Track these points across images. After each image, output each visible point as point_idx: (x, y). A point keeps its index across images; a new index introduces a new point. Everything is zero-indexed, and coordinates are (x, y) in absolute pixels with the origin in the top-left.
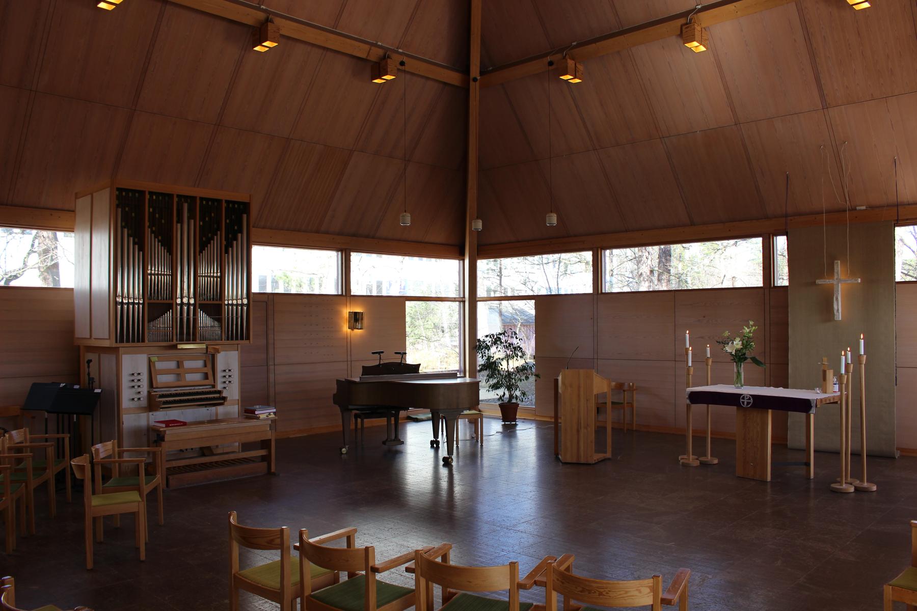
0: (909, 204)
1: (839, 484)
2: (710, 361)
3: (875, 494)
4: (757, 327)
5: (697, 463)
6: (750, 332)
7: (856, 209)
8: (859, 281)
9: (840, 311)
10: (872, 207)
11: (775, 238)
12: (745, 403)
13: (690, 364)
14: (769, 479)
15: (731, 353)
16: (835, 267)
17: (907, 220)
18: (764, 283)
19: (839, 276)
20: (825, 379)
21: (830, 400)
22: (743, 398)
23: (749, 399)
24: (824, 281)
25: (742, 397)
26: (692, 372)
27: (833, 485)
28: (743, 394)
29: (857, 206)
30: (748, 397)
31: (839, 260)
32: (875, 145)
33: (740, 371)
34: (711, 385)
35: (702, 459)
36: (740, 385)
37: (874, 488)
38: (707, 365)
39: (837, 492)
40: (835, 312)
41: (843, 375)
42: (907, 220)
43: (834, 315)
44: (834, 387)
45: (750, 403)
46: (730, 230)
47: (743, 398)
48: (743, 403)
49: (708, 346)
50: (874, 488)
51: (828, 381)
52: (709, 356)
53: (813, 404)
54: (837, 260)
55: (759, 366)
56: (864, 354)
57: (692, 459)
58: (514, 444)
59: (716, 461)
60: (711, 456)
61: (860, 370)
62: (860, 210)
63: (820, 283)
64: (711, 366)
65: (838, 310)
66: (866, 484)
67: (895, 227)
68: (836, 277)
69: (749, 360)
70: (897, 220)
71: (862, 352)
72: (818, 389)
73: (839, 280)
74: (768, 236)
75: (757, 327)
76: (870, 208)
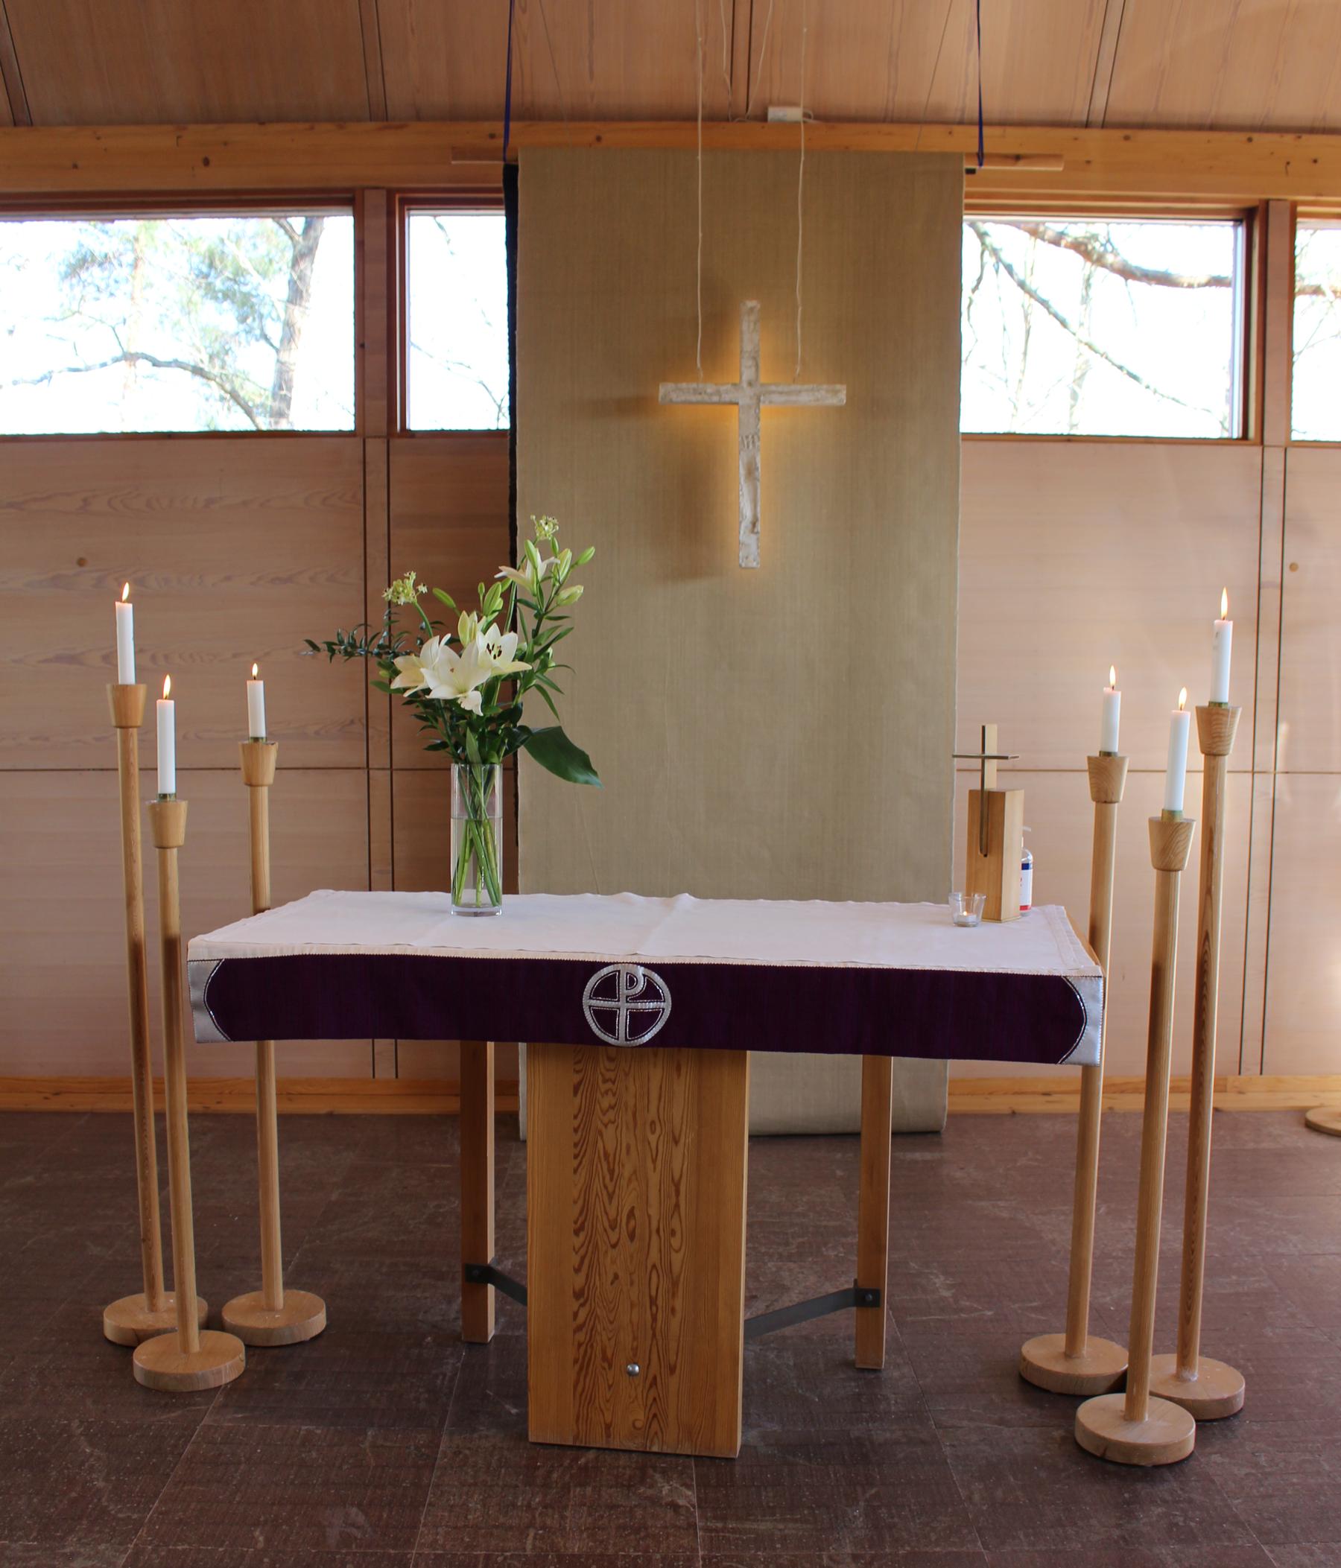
2: (271, 758)
4: (591, 552)
7: (763, 118)
10: (823, 118)
12: (622, 1022)
13: (168, 781)
22: (607, 989)
23: (651, 992)
24: (696, 392)
25: (593, 981)
26: (178, 831)
28: (596, 966)
29: (771, 103)
30: (641, 986)
38: (252, 784)
45: (653, 1016)
46: (206, 162)
48: (607, 1019)
49: (255, 670)
55: (564, 775)
58: (317, 223)
64: (271, 789)
68: (748, 374)
74: (383, 201)
76: (817, 118)
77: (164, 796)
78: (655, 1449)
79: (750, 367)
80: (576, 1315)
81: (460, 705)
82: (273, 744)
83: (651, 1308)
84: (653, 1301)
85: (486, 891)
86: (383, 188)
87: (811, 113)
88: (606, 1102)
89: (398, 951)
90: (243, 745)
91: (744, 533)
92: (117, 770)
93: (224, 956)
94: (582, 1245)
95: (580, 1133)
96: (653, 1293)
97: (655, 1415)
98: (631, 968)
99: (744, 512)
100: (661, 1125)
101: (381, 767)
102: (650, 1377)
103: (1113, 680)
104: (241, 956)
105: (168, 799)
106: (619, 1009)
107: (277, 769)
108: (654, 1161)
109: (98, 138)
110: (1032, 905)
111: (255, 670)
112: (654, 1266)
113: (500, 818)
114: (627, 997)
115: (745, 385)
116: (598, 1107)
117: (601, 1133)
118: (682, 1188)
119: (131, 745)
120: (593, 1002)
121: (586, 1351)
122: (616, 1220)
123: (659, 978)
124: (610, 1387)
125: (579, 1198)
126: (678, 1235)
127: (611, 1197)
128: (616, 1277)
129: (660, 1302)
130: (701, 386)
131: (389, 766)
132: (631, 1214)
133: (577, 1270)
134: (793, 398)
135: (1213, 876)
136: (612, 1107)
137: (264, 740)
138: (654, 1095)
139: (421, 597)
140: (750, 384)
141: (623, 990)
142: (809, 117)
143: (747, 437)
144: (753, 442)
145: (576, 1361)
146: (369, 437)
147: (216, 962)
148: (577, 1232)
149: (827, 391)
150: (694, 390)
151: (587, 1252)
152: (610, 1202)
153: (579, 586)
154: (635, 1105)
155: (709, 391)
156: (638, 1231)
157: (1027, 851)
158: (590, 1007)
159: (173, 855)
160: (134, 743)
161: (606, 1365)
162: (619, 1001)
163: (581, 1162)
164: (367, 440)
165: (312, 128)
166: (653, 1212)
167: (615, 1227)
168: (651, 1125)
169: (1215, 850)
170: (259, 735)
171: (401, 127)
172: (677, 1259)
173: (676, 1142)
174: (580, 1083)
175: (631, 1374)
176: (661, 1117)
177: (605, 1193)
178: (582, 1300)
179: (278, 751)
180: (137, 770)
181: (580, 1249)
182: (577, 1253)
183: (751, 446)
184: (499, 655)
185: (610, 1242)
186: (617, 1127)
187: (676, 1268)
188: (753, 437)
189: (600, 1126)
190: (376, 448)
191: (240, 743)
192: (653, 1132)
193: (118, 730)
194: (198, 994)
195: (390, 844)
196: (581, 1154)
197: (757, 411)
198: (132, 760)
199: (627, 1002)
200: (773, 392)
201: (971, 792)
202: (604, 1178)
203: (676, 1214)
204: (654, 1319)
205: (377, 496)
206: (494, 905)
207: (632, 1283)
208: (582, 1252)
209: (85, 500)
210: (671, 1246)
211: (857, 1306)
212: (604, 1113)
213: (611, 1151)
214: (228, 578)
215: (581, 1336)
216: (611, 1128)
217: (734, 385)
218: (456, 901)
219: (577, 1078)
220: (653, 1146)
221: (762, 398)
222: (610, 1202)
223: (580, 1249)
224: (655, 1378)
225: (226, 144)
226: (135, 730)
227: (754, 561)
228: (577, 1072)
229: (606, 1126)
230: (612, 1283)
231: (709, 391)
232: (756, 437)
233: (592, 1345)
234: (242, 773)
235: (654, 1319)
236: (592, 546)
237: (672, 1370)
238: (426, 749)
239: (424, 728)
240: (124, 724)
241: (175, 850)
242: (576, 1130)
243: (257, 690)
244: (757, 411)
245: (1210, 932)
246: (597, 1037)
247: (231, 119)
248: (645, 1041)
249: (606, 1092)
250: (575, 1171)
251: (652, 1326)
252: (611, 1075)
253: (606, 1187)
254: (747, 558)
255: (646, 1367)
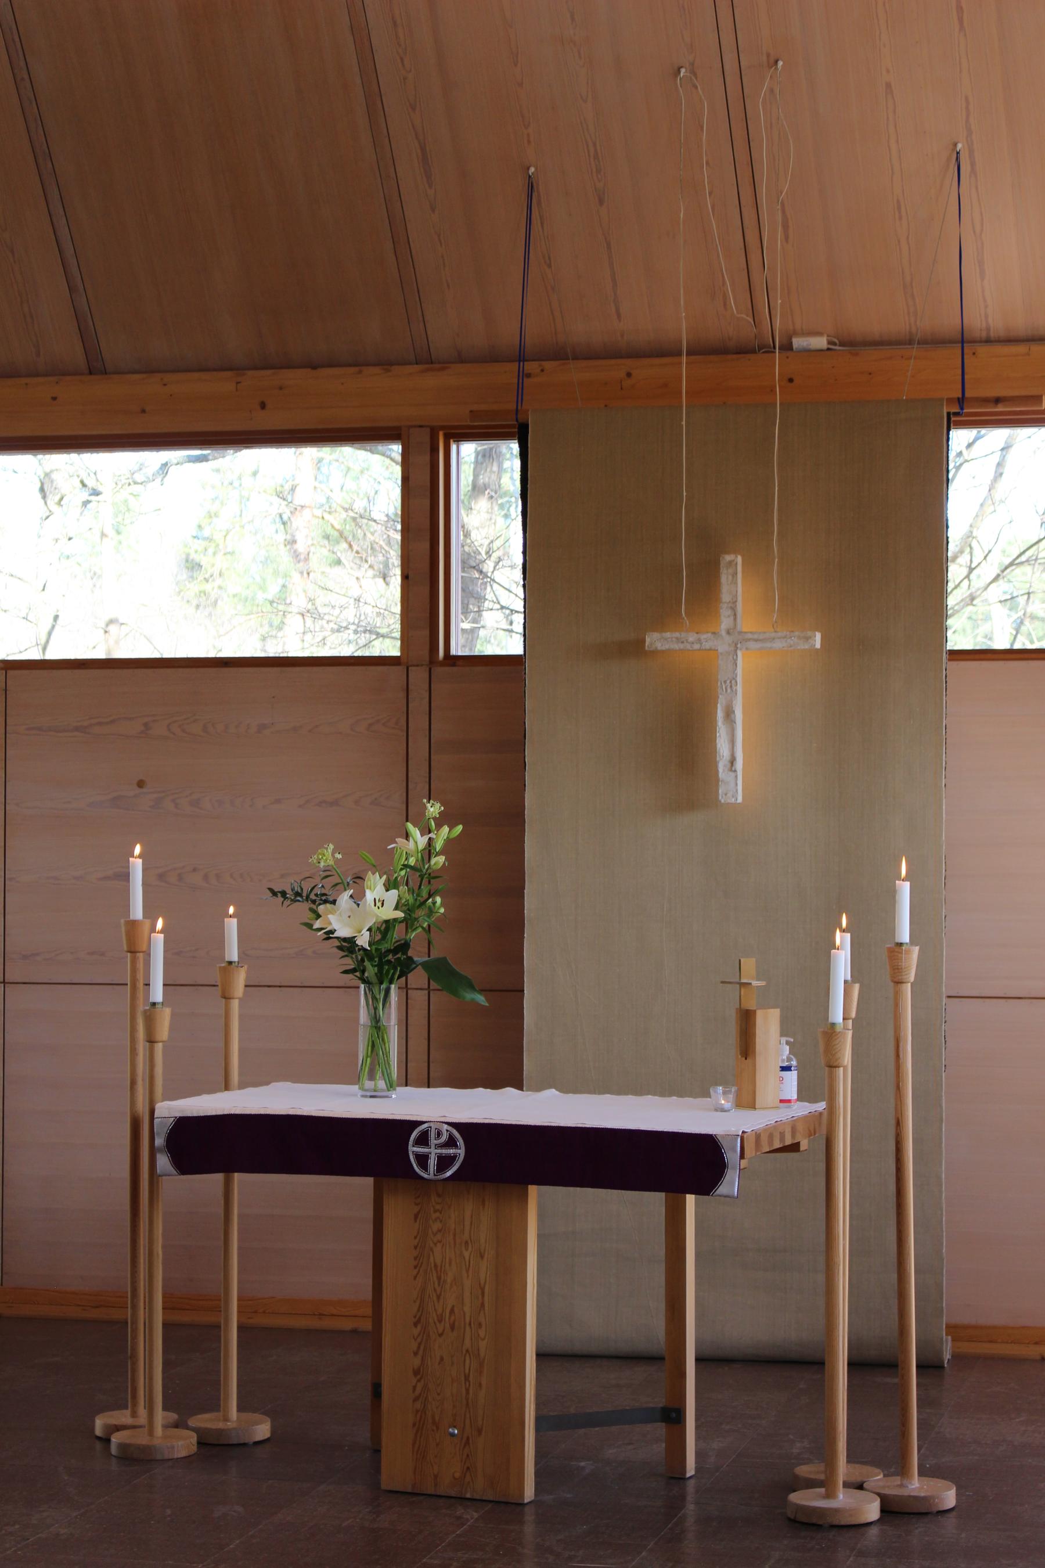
0: (988, 341)
1: (823, 1490)
2: (240, 979)
3: (950, 1523)
4: (460, 828)
5: (184, 1444)
6: (429, 850)
8: (818, 645)
9: (739, 765)
11: (454, 447)
12: (432, 1162)
13: (157, 994)
14: (529, 1493)
15: (348, 945)
16: (724, 579)
17: (997, 401)
18: (406, 639)
19: (739, 621)
20: (747, 1047)
21: (782, 1135)
22: (423, 1139)
23: (451, 1142)
24: (678, 640)
25: (415, 1134)
26: (163, 1031)
27: (797, 1498)
29: (795, 333)
30: (444, 1138)
31: (735, 552)
32: (888, 85)
33: (384, 1022)
34: (242, 1086)
35: (204, 1421)
36: (381, 1084)
37: (949, 1498)
38: (227, 997)
39: (818, 1527)
40: (721, 770)
41: (839, 1028)
42: (997, 401)
43: (717, 780)
44: (782, 1079)
46: (263, 406)
47: (423, 1139)
48: (423, 1160)
49: (231, 910)
50: (949, 1498)
51: (760, 1060)
52: (235, 957)
53: (731, 1156)
54: (728, 553)
56: (913, 940)
57: (165, 1427)
59: (263, 1430)
60: (240, 1409)
61: (896, 1005)
62: (808, 352)
63: (660, 646)
65: (732, 761)
66: (916, 1485)
67: (949, 430)
68: (725, 623)
69: (418, 977)
70: (961, 401)
71: (904, 934)
72: (720, 1089)
73: (739, 640)
75: (460, 828)
77: (154, 1004)
78: (468, 1496)
79: (729, 616)
80: (414, 1388)
81: (355, 941)
82: (242, 967)
83: (465, 1383)
84: (467, 1378)
85: (383, 1081)
86: (426, 426)
87: (836, 341)
88: (436, 1226)
89: (291, 1112)
90: (220, 967)
91: (724, 770)
92: (127, 984)
93: (178, 1115)
94: (419, 1334)
95: (418, 1250)
96: (467, 1371)
97: (468, 1468)
98: (438, 1126)
99: (721, 751)
100: (472, 1244)
101: (419, 987)
102: (465, 1439)
103: (844, 924)
104: (190, 1115)
105: (157, 1006)
106: (431, 1153)
107: (246, 986)
108: (467, 1271)
109: (165, 385)
110: (798, 1100)
111: (231, 910)
112: (467, 1351)
113: (395, 1025)
114: (436, 1145)
115: (723, 633)
116: (430, 1230)
117: (432, 1250)
118: (486, 1291)
119: (138, 965)
120: (415, 1149)
121: (421, 1417)
122: (442, 1315)
123: (457, 1132)
124: (437, 1445)
125: (417, 1298)
126: (484, 1328)
127: (438, 1297)
128: (442, 1359)
129: (471, 1378)
130: (683, 635)
131: (426, 987)
132: (452, 1311)
133: (416, 1354)
134: (768, 645)
135: (900, 1075)
136: (439, 1231)
137: (237, 964)
138: (467, 1223)
139: (337, 861)
140: (728, 632)
141: (433, 1141)
142: (835, 344)
143: (725, 682)
144: (731, 687)
145: (414, 1425)
146: (411, 666)
147: (173, 1119)
148: (415, 1325)
149: (799, 638)
150: (677, 638)
151: (422, 1339)
152: (438, 1302)
153: (441, 856)
154: (455, 1229)
155: (691, 639)
156: (457, 1324)
157: (792, 1056)
158: (413, 1152)
159: (159, 1047)
160: (141, 965)
161: (435, 1428)
162: (430, 1148)
163: (419, 1271)
164: (410, 668)
165: (360, 372)
166: (467, 1309)
167: (442, 1320)
168: (465, 1244)
169: (901, 1056)
170: (233, 960)
171: (443, 369)
172: (483, 1345)
173: (482, 1257)
174: (419, 1212)
175: (452, 1435)
176: (472, 1238)
177: (435, 1295)
178: (419, 1377)
179: (248, 973)
180: (142, 985)
181: (417, 1337)
182: (415, 1340)
183: (729, 690)
184: (382, 906)
185: (438, 1332)
186: (443, 1245)
187: (482, 1354)
188: (731, 682)
189: (432, 1245)
190: (419, 676)
191: (218, 965)
192: (467, 1250)
193: (129, 954)
194: (159, 1141)
195: (426, 1064)
196: (419, 1265)
197: (735, 657)
198: (138, 977)
199: (436, 1149)
200: (749, 640)
201: (737, 1009)
202: (434, 1284)
203: (482, 1312)
204: (467, 1391)
205: (419, 722)
206: (389, 1091)
207: (453, 1364)
208: (419, 1340)
209: (146, 725)
210: (479, 1335)
211: (665, 1422)
212: (435, 1234)
213: (439, 1262)
214: (278, 801)
215: (418, 1405)
216: (439, 1245)
217: (714, 633)
218: (362, 1089)
219: (416, 1209)
220: (467, 1258)
221: (739, 646)
222: (438, 1302)
223: (417, 1337)
224: (468, 1438)
225: (281, 388)
226: (141, 954)
227: (733, 797)
228: (417, 1204)
229: (435, 1244)
230: (439, 1364)
231: (691, 639)
232: (733, 682)
233: (425, 1413)
234: (219, 988)
235: (467, 1391)
236: (460, 824)
237: (480, 1431)
238: (341, 973)
239: (343, 957)
240: (133, 950)
241: (160, 1045)
242: (416, 1248)
243: (232, 926)
244: (735, 657)
245: (900, 1118)
246: (417, 1173)
247: (288, 365)
248: (447, 1176)
249: (436, 1220)
250: (415, 1278)
251: (466, 1396)
252: (438, 1207)
253: (435, 1290)
254: (726, 795)
255: (462, 1431)
